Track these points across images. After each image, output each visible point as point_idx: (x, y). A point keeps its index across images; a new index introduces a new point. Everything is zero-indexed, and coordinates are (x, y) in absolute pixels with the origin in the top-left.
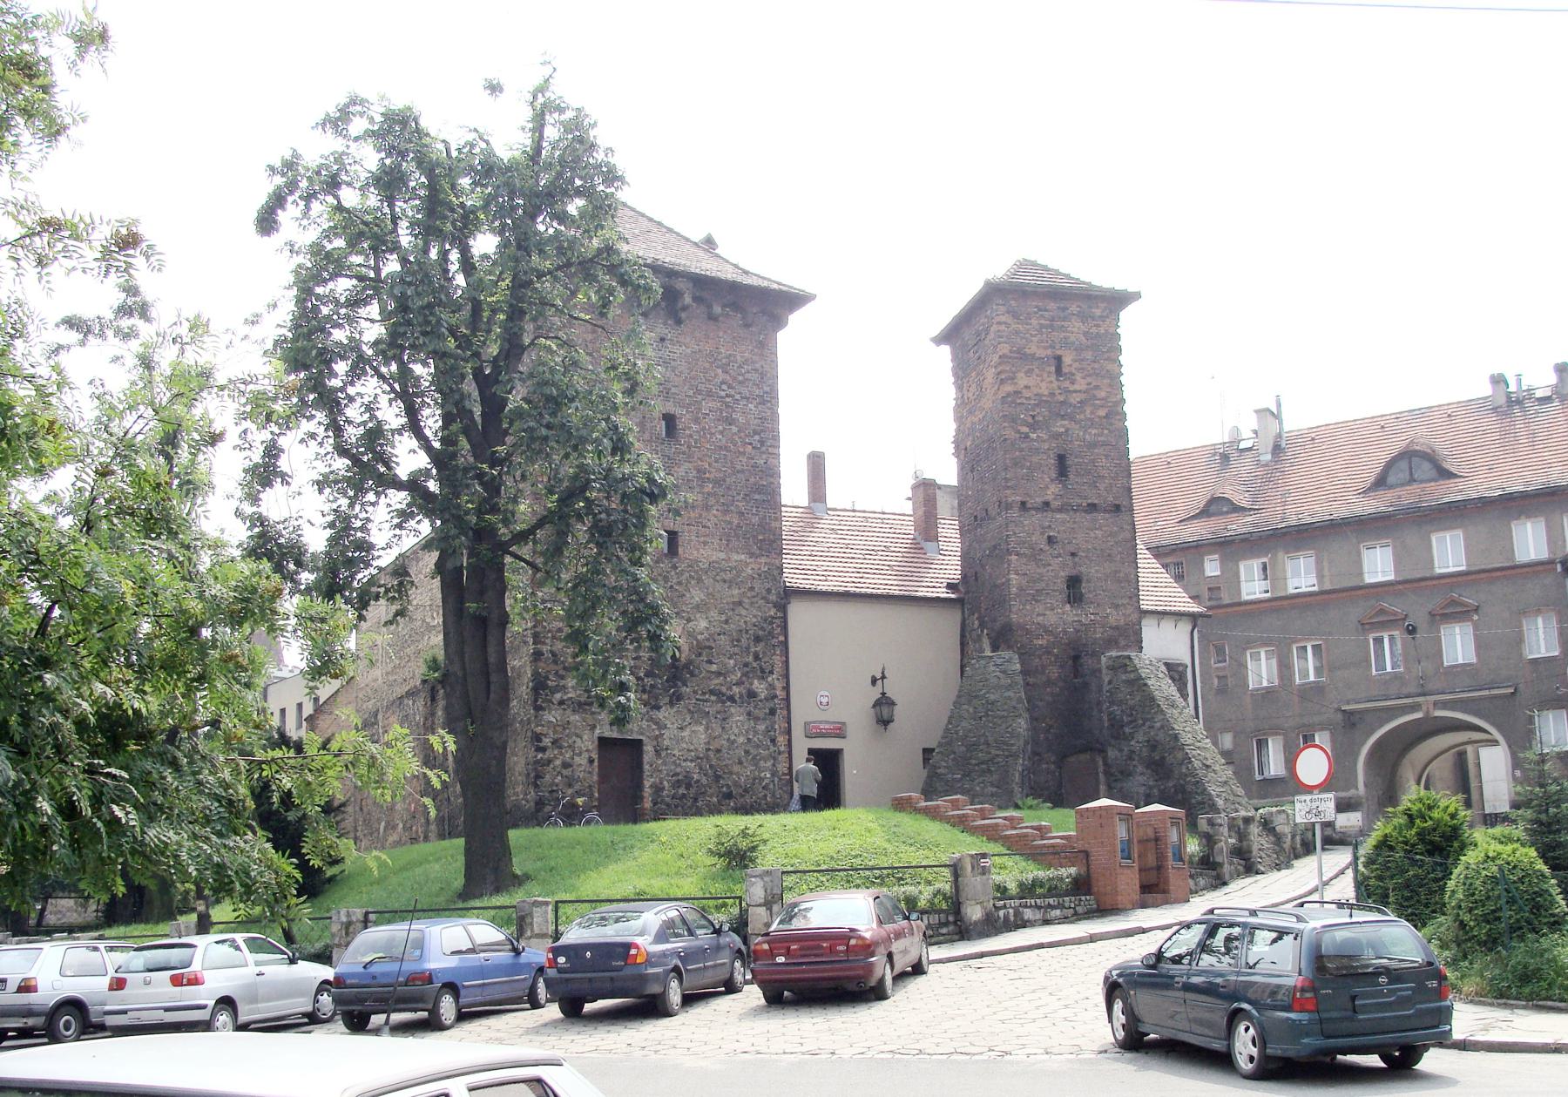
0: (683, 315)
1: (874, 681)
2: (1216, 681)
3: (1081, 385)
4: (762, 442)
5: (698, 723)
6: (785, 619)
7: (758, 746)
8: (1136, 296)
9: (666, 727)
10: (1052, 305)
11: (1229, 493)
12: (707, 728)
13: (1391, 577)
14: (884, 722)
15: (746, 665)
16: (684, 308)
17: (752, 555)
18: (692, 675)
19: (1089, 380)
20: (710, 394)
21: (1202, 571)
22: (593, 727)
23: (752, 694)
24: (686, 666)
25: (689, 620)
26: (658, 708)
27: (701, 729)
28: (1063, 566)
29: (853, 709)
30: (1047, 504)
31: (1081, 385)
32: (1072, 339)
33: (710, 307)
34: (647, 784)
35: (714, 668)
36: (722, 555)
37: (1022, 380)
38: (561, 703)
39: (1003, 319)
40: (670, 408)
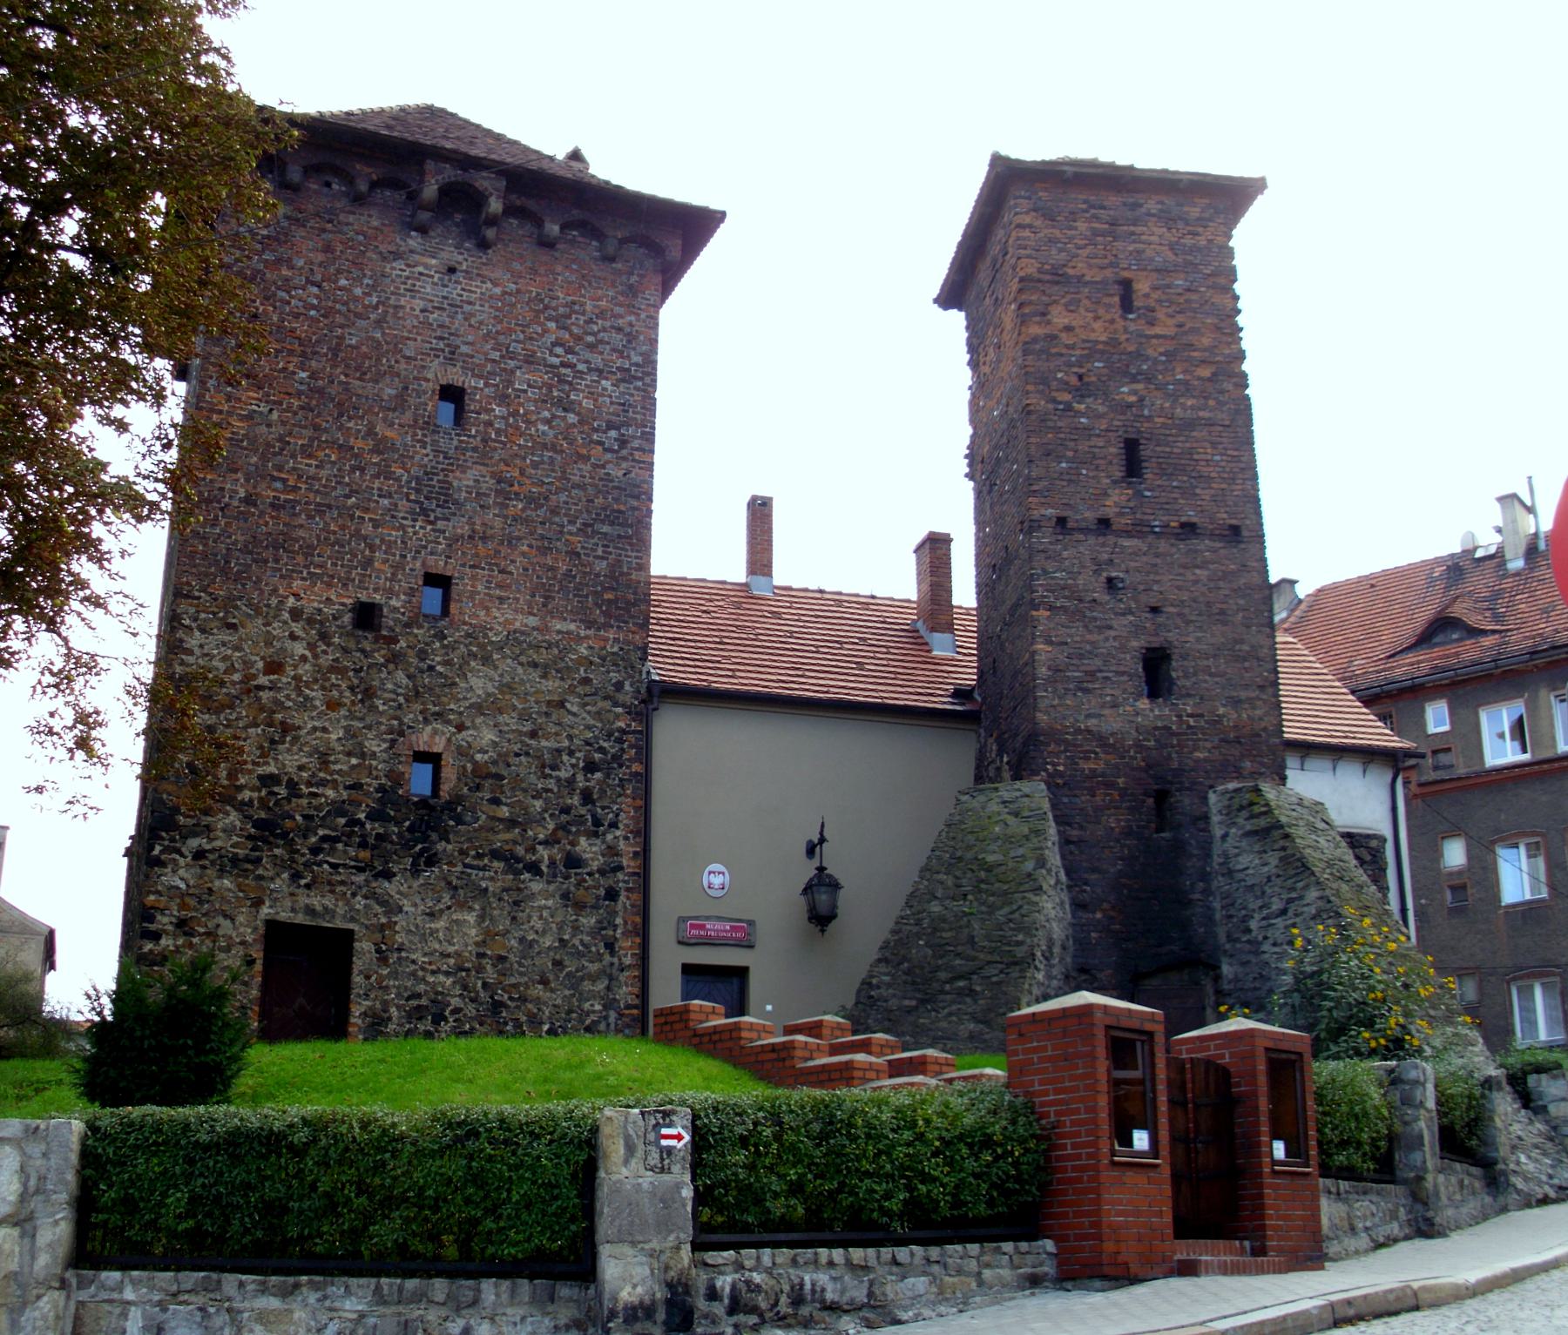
0: (490, 233)
1: (811, 850)
2: (1448, 895)
3: (1166, 327)
4: (623, 442)
5: (464, 906)
6: (646, 736)
7: (580, 955)
9: (400, 910)
10: (1113, 200)
11: (1458, 610)
12: (482, 918)
14: (821, 919)
15: (566, 810)
16: (492, 221)
17: (589, 624)
18: (459, 821)
19: (1180, 318)
20: (530, 360)
21: (1422, 724)
22: (258, 903)
23: (573, 862)
24: (450, 806)
25: (461, 728)
26: (388, 875)
27: (471, 918)
28: (1137, 630)
29: (776, 905)
30: (1104, 523)
31: (1166, 327)
32: (1149, 253)
33: (539, 223)
34: (356, 1011)
36: (533, 621)
37: (1059, 317)
38: (199, 855)
39: (1027, 220)
40: (455, 376)
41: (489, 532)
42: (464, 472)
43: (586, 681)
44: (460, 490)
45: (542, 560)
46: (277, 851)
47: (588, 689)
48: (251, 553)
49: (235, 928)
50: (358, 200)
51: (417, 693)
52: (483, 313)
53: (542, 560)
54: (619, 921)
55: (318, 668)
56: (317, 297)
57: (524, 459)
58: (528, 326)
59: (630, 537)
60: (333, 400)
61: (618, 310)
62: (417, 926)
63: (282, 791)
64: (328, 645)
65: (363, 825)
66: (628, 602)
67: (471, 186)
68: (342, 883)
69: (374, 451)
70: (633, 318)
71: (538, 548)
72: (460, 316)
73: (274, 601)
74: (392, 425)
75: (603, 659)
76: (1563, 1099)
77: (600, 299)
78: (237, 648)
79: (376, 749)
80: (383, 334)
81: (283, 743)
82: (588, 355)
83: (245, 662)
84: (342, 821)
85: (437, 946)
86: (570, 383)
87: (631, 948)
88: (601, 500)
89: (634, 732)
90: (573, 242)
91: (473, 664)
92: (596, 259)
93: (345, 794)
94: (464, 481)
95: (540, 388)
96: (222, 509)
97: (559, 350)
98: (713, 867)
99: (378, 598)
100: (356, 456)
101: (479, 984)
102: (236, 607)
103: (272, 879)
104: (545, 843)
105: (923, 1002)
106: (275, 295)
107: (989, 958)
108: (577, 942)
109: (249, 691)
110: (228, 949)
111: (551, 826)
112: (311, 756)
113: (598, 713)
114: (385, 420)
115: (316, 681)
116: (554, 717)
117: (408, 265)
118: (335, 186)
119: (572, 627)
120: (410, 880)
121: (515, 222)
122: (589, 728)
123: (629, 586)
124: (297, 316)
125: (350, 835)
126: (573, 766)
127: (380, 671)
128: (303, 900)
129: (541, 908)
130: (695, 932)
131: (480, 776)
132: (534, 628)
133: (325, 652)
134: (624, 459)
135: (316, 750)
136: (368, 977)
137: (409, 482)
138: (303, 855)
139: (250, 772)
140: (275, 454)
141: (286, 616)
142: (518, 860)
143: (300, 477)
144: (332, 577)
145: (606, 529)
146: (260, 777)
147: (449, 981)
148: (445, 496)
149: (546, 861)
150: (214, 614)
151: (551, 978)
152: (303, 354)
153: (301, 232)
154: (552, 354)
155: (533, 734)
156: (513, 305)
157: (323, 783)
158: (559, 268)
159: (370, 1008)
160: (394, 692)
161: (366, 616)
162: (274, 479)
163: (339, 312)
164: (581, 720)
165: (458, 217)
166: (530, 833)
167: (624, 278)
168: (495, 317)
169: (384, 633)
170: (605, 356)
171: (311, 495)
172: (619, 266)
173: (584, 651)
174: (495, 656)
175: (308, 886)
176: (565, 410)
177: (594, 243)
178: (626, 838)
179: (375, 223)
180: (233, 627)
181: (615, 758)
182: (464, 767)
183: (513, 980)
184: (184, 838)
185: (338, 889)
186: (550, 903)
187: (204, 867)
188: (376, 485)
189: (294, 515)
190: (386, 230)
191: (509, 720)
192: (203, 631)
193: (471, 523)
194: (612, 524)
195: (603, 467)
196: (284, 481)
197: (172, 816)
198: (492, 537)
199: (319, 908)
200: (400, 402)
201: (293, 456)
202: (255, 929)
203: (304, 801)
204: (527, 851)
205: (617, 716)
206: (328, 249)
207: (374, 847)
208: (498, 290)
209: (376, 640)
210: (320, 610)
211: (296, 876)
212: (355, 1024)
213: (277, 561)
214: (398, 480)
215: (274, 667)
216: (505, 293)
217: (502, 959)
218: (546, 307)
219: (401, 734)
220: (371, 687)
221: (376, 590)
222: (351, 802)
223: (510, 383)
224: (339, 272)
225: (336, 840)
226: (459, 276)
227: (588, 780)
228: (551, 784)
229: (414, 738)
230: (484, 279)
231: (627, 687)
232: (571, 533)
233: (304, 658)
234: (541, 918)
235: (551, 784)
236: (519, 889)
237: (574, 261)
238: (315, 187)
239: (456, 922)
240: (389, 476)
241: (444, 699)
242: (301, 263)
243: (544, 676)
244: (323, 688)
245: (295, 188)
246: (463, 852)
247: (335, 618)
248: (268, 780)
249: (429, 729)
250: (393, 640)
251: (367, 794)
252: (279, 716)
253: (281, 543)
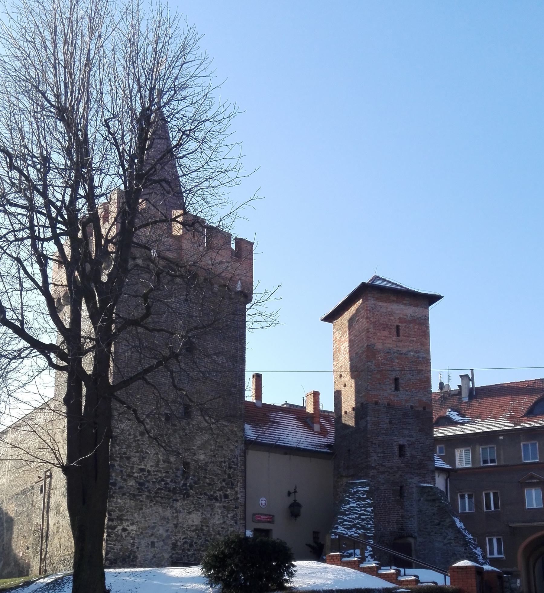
1: (289, 494)
6: (245, 457)
8: (322, 320)
23: (226, 496)
76: (3, 433)
93: (164, 475)
98: (262, 499)
104: (218, 490)
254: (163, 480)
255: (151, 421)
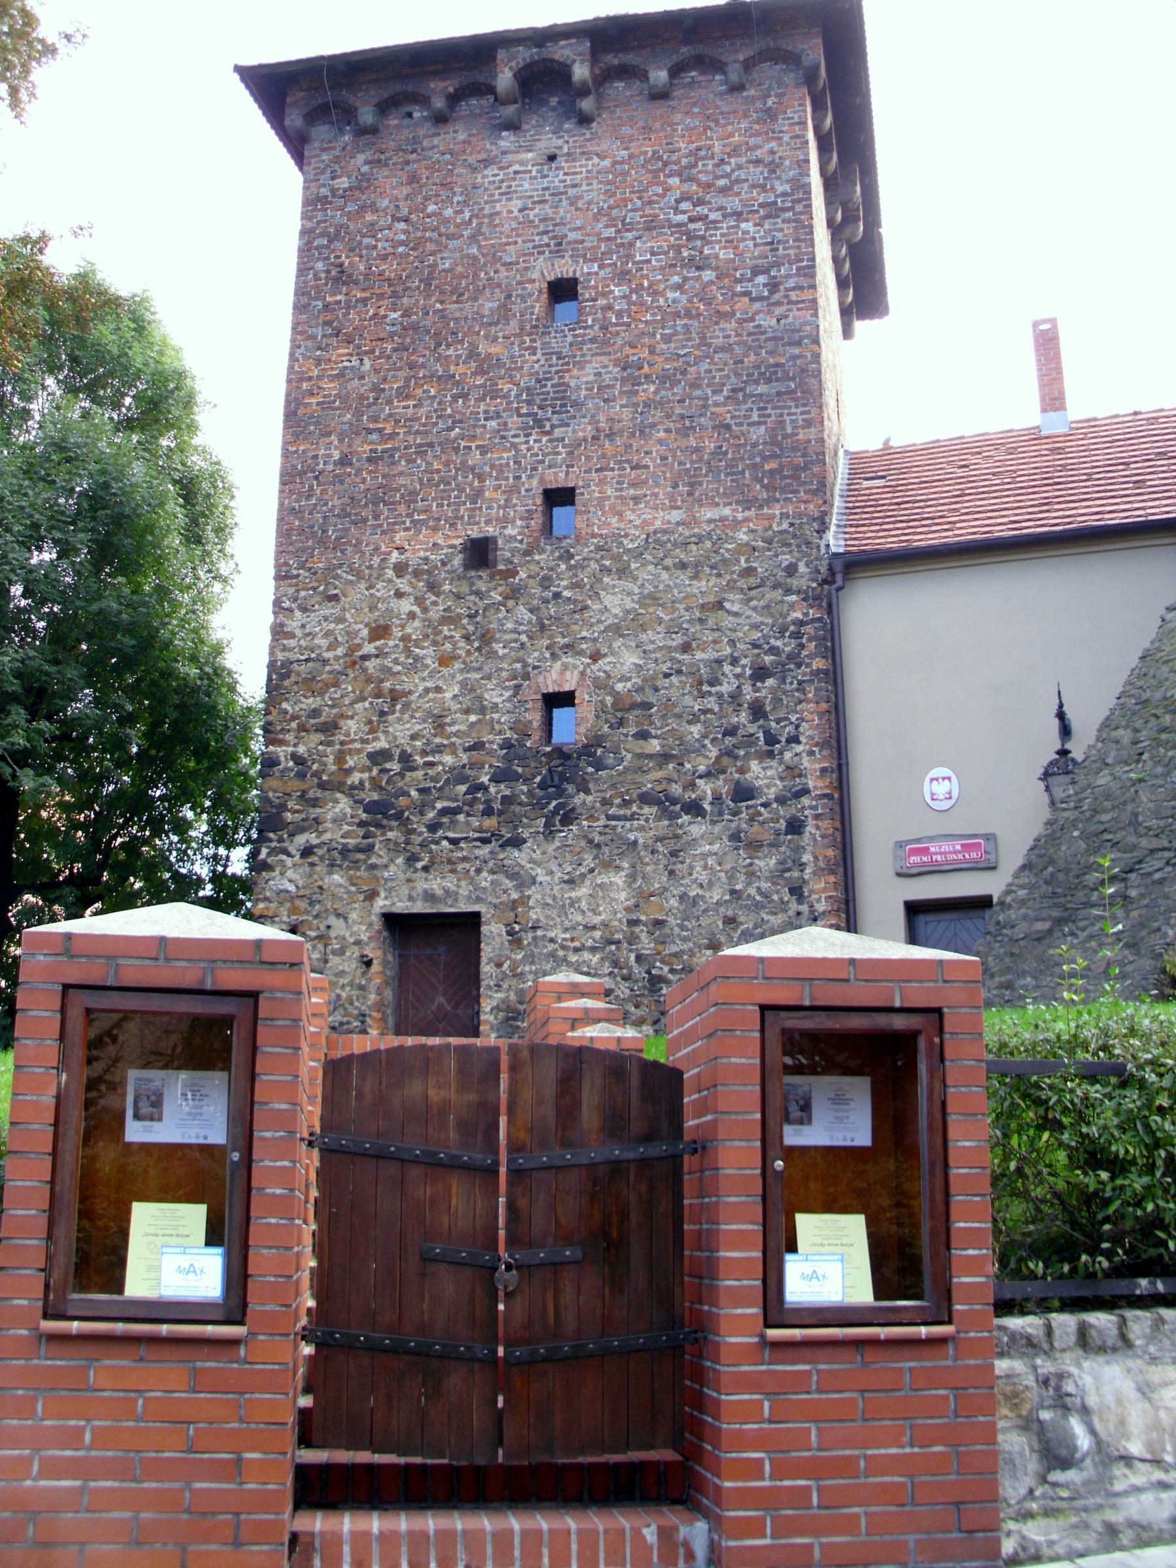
0: (586, 104)
5: (609, 865)
7: (758, 906)
8: (239, 69)
9: (533, 881)
12: (632, 877)
13: (819, 41)
15: (731, 731)
17: (747, 504)
18: (599, 766)
20: (651, 225)
22: (371, 895)
23: (744, 793)
25: (596, 657)
26: (517, 842)
27: (619, 879)
33: (644, 76)
34: (486, 1005)
35: (654, 746)
36: (676, 515)
38: (307, 852)
40: (564, 268)
41: (617, 427)
42: (582, 368)
43: (749, 572)
44: (578, 388)
45: (683, 443)
46: (391, 835)
47: (752, 581)
48: (348, 515)
49: (348, 927)
50: (441, 119)
51: (543, 627)
52: (593, 192)
53: (683, 443)
54: (806, 858)
55: (428, 623)
56: (405, 232)
57: (654, 335)
58: (646, 190)
59: (794, 392)
60: (428, 332)
61: (752, 141)
62: (554, 898)
63: (395, 766)
64: (438, 595)
65: (485, 789)
66: (797, 469)
67: (552, 60)
68: (464, 859)
69: (480, 372)
70: (773, 144)
71: (678, 431)
72: (565, 203)
73: (376, 561)
74: (495, 339)
75: (769, 541)
77: (731, 135)
78: (340, 620)
79: (498, 700)
80: (480, 247)
81: (393, 712)
82: (722, 201)
83: (348, 633)
84: (463, 788)
85: (579, 918)
86: (703, 238)
87: (824, 890)
88: (752, 358)
89: (813, 621)
90: (692, 84)
91: (606, 580)
92: (721, 94)
93: (465, 758)
94: (581, 379)
95: (666, 253)
96: (316, 478)
97: (685, 206)
99: (490, 530)
100: (458, 383)
101: (633, 958)
102: (337, 577)
103: (386, 866)
104: (708, 775)
105: (1060, 922)
106: (360, 243)
107: (1155, 843)
108: (752, 891)
109: (355, 663)
110: (341, 952)
111: (713, 753)
112: (424, 721)
113: (768, 607)
114: (486, 337)
115: (426, 636)
116: (711, 623)
117: (500, 169)
118: (416, 115)
119: (727, 511)
120: (545, 845)
121: (621, 85)
122: (756, 627)
123: (795, 449)
124: (384, 258)
125: (471, 804)
126: (737, 676)
127: (498, 610)
128: (421, 886)
129: (705, 856)
130: (915, 859)
131: (623, 710)
132: (678, 524)
133: (435, 603)
134: (778, 304)
135: (429, 713)
136: (499, 965)
137: (518, 396)
138: (421, 834)
139: (358, 751)
140: (369, 406)
141: (390, 573)
142: (674, 801)
143: (397, 422)
144: (438, 519)
145: (762, 389)
146: (371, 756)
147: (595, 959)
148: (563, 403)
149: (709, 797)
150: (314, 589)
151: (723, 939)
152: (395, 295)
153: (385, 172)
154: (677, 211)
155: (686, 648)
156: (626, 174)
157: (439, 749)
158: (678, 117)
159: (503, 1001)
160: (515, 631)
161: (480, 553)
162: (370, 431)
163: (430, 240)
164: (745, 620)
165: (554, 101)
166: (688, 766)
167: (759, 105)
168: (606, 192)
169: (501, 567)
170: (744, 196)
171: (411, 438)
172: (752, 92)
173: (742, 536)
174: (633, 566)
175: (425, 869)
176: (699, 268)
177: (717, 77)
178: (811, 753)
179: (462, 136)
180: (335, 598)
181: (791, 657)
182: (602, 702)
183: (674, 949)
184: (292, 835)
185: (460, 867)
186: (716, 847)
187: (312, 865)
188: (483, 407)
189: (393, 463)
190: (473, 140)
191: (655, 637)
192: (304, 610)
193: (594, 421)
194: (769, 381)
195: (752, 319)
196: (380, 430)
197: (279, 814)
198: (621, 431)
199: (439, 892)
200: (504, 313)
201: (389, 402)
202: (371, 925)
203: (419, 774)
204: (685, 788)
205: (792, 606)
206: (413, 179)
207: (501, 813)
208: (607, 163)
209: (492, 577)
210: (426, 559)
211: (412, 859)
212: (487, 1022)
213: (376, 517)
214: (506, 396)
215: (379, 632)
216: (615, 163)
217: (659, 923)
218: (665, 165)
219: (526, 677)
220: (488, 631)
221: (487, 523)
222: (472, 765)
223: (629, 257)
224: (426, 199)
225: (455, 812)
226: (561, 162)
227: (757, 690)
228: (711, 703)
229: (541, 679)
230: (588, 155)
231: (802, 568)
232: (716, 404)
233: (412, 616)
234: (705, 867)
235: (711, 703)
236: (676, 836)
237: (695, 104)
238: (396, 122)
239: (601, 886)
240: (495, 394)
241: (574, 627)
242: (385, 203)
243: (696, 577)
244: (435, 643)
245: (373, 131)
246: (605, 802)
247: (444, 564)
248: (379, 757)
249: (557, 665)
250: (513, 573)
251: (490, 753)
252: (387, 684)
253: (380, 497)
254: (462, 779)
255: (91, 768)
